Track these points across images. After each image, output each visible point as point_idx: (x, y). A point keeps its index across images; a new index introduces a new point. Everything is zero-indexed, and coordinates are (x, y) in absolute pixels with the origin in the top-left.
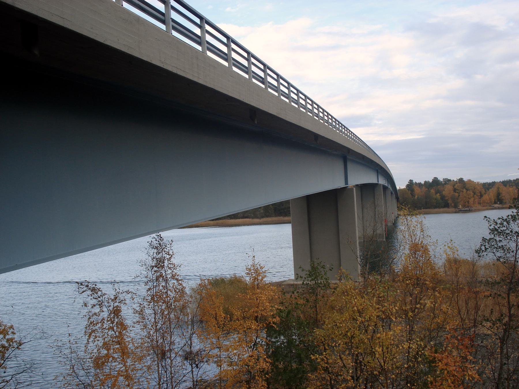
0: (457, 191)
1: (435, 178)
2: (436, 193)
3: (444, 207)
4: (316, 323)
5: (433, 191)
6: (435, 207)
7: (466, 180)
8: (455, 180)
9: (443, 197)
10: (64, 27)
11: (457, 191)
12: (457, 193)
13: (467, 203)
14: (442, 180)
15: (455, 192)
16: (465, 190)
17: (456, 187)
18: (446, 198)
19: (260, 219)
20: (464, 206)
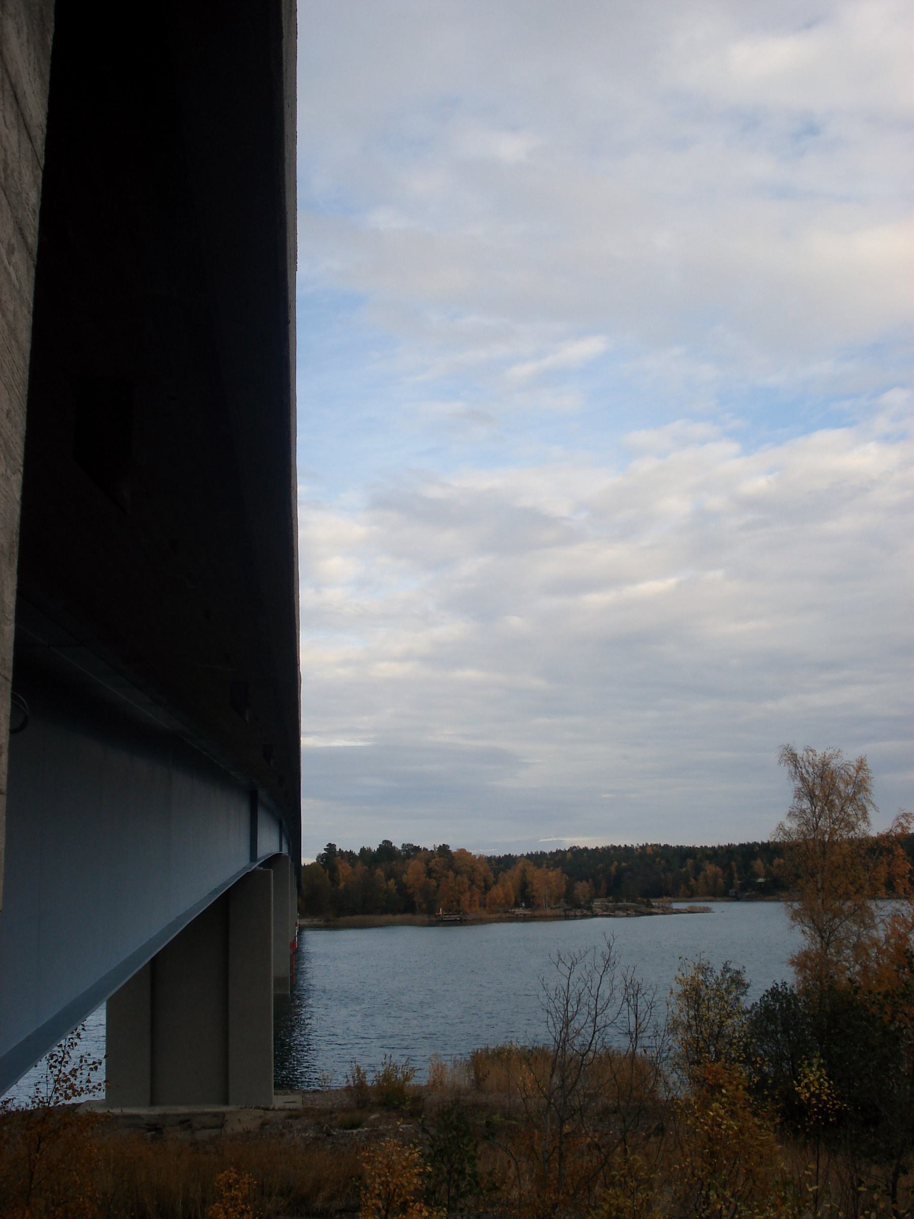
1: (385, 842)
2: (388, 878)
3: (405, 911)
5: (380, 872)
12: (435, 878)
14: (399, 847)
18: (410, 891)
20: (448, 910)
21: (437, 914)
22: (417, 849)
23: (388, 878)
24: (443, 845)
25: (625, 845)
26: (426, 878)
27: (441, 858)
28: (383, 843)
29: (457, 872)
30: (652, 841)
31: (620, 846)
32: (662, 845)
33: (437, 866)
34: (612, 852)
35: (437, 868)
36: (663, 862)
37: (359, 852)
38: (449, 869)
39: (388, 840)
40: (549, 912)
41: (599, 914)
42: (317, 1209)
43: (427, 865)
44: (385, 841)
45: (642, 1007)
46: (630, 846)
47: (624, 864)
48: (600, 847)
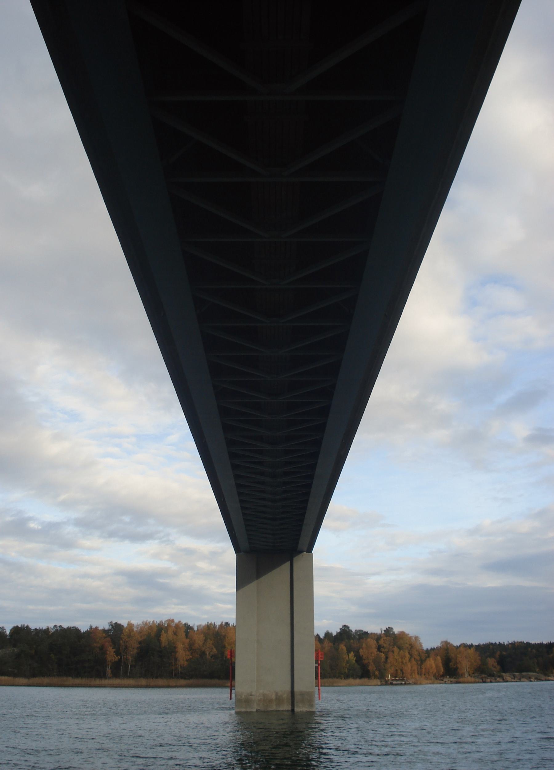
0: (383, 650)
1: (345, 626)
2: (349, 651)
3: (361, 677)
4: (169, 639)
5: (343, 647)
6: (347, 677)
7: (397, 633)
8: (379, 632)
9: (359, 659)
10: (73, 632)
11: (383, 650)
12: (383, 653)
13: (323, 685)
14: (354, 631)
15: (380, 652)
16: (396, 649)
17: (381, 642)
18: (366, 661)
19: (29, 679)
20: (395, 676)
21: (387, 679)
22: (366, 633)
23: (349, 651)
24: (389, 628)
25: (499, 643)
26: (377, 651)
27: (388, 638)
28: (343, 627)
29: (400, 648)
30: (520, 640)
31: (496, 643)
32: (525, 642)
33: (385, 643)
34: (491, 647)
35: (385, 645)
36: (534, 650)
37: (324, 635)
38: (394, 646)
39: (347, 625)
40: (470, 679)
41: (509, 681)
42: (141, 625)
43: (378, 642)
44: (344, 625)
45: (446, 759)
46: (503, 643)
47: (504, 653)
48: (481, 644)
